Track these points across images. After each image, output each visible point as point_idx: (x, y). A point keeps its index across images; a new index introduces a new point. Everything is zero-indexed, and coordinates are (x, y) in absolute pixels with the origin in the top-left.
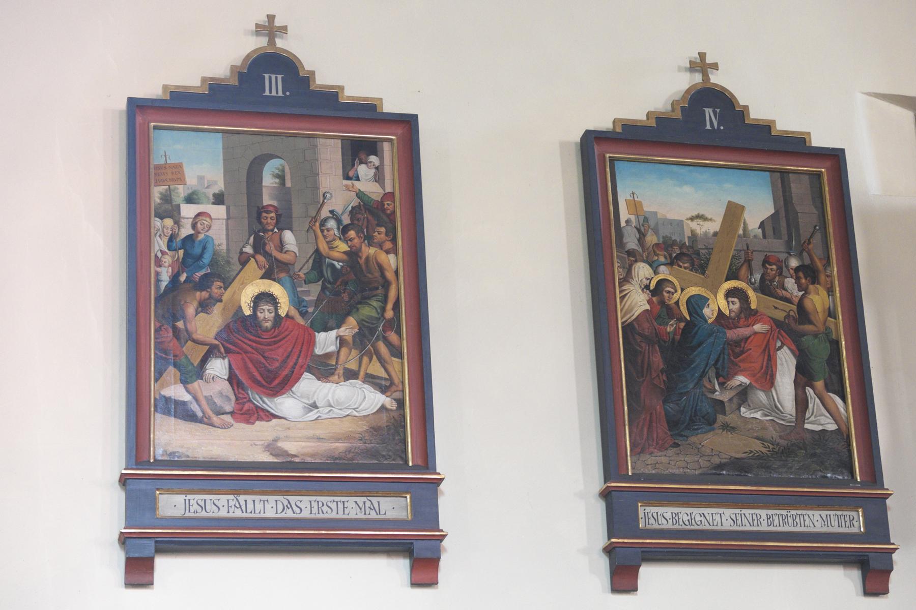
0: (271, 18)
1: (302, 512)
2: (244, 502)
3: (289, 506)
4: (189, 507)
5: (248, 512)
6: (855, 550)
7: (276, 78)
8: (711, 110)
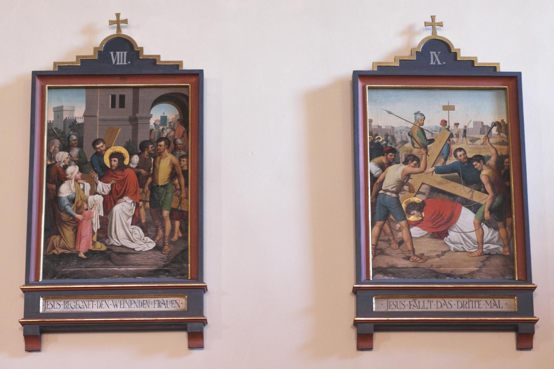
1: (452, 308)
2: (498, 302)
3: (445, 304)
5: (438, 308)
6: (457, 322)
7: (123, 54)
8: (435, 53)
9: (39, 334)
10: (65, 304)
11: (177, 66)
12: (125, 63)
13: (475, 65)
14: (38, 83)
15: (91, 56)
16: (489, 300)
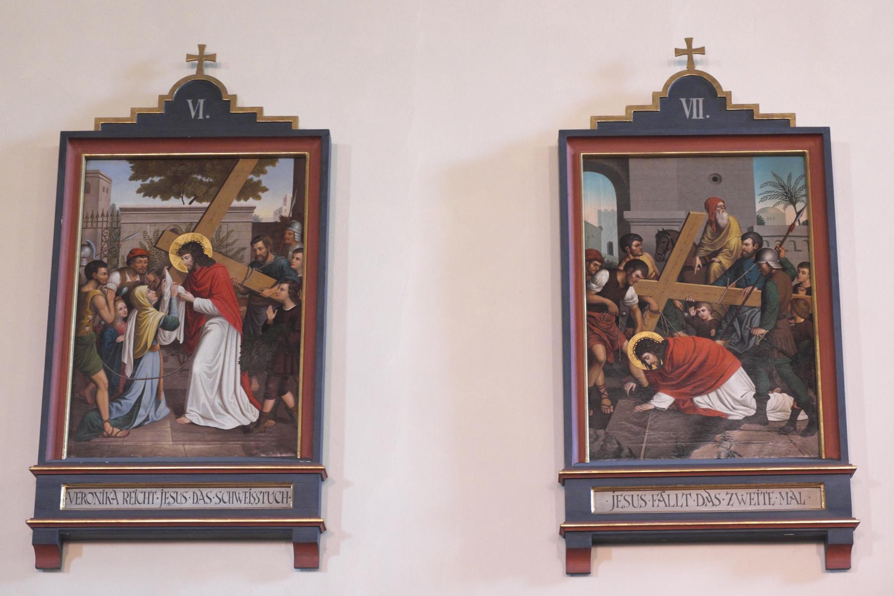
0: (202, 47)
2: (799, 494)
4: (617, 503)
7: (698, 101)
9: (58, 543)
10: (83, 496)
11: (785, 121)
12: (701, 117)
13: (755, 118)
14: (69, 148)
15: (127, 119)
16: (784, 491)
